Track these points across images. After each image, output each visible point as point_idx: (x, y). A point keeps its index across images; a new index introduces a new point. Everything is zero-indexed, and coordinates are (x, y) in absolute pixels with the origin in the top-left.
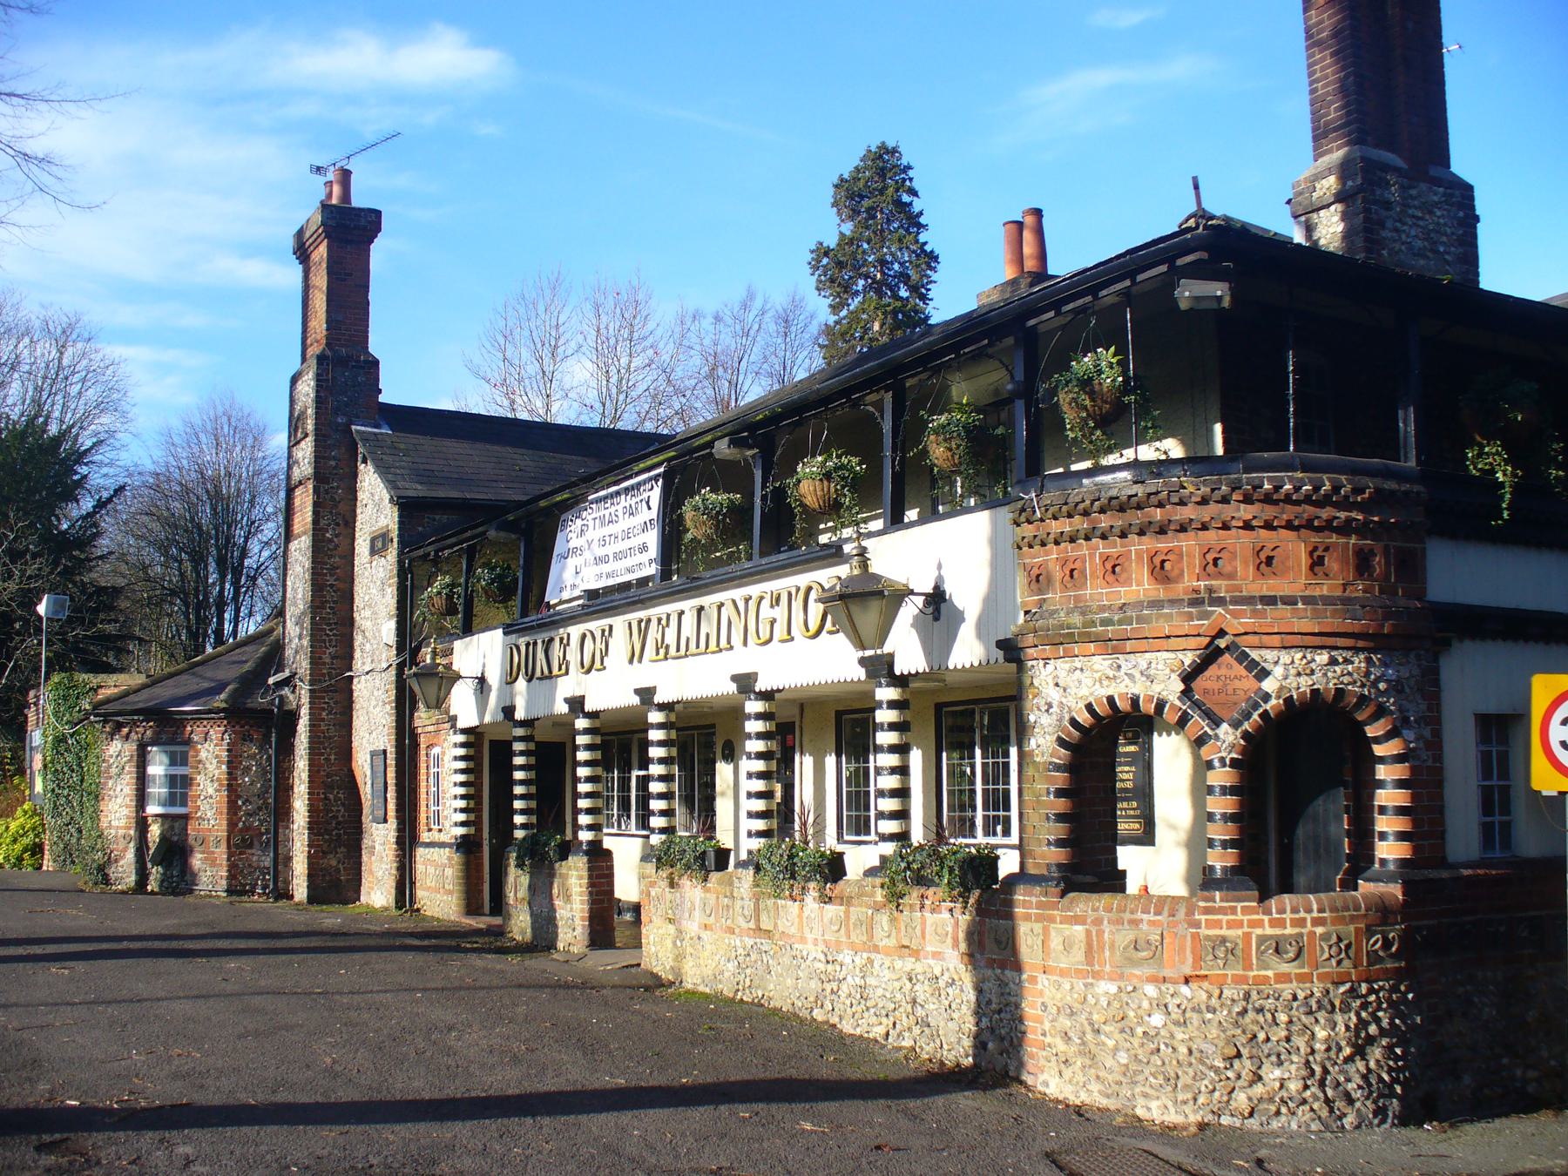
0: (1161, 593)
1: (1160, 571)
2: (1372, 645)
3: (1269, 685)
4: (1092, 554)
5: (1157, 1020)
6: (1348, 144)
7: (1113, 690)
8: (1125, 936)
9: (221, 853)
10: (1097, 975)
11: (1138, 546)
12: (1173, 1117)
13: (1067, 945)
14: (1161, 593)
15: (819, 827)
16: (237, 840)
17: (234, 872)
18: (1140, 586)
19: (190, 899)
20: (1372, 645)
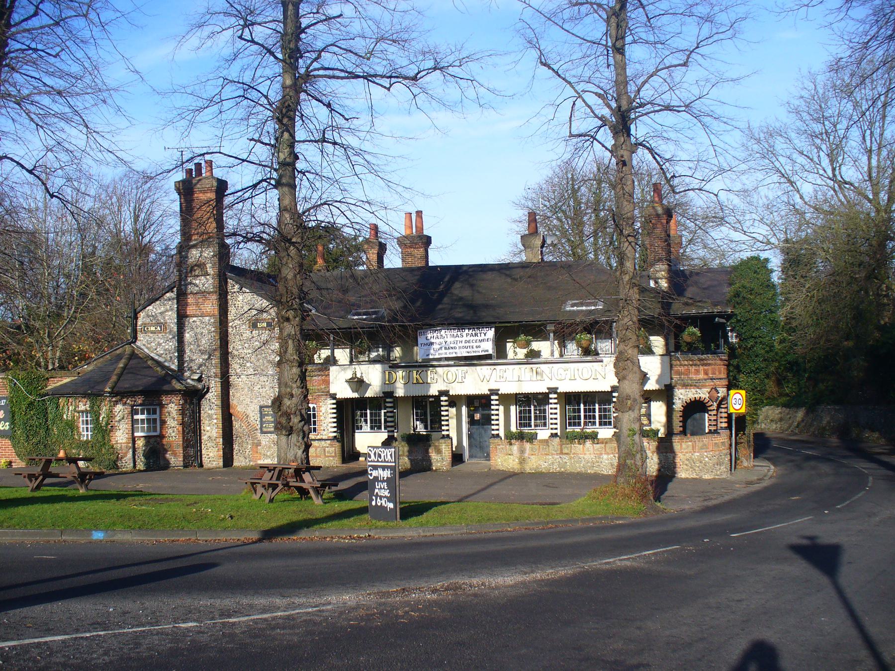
0: (706, 377)
1: (706, 373)
2: (875, 456)
3: (719, 395)
4: (693, 369)
5: (707, 459)
6: (792, 404)
7: (696, 396)
8: (701, 444)
9: (180, 451)
10: (695, 452)
11: (701, 368)
12: (710, 478)
13: (688, 447)
14: (706, 377)
15: (191, 452)
16: (185, 444)
17: (185, 457)
18: (701, 376)
19: (169, 471)
20: (875, 456)
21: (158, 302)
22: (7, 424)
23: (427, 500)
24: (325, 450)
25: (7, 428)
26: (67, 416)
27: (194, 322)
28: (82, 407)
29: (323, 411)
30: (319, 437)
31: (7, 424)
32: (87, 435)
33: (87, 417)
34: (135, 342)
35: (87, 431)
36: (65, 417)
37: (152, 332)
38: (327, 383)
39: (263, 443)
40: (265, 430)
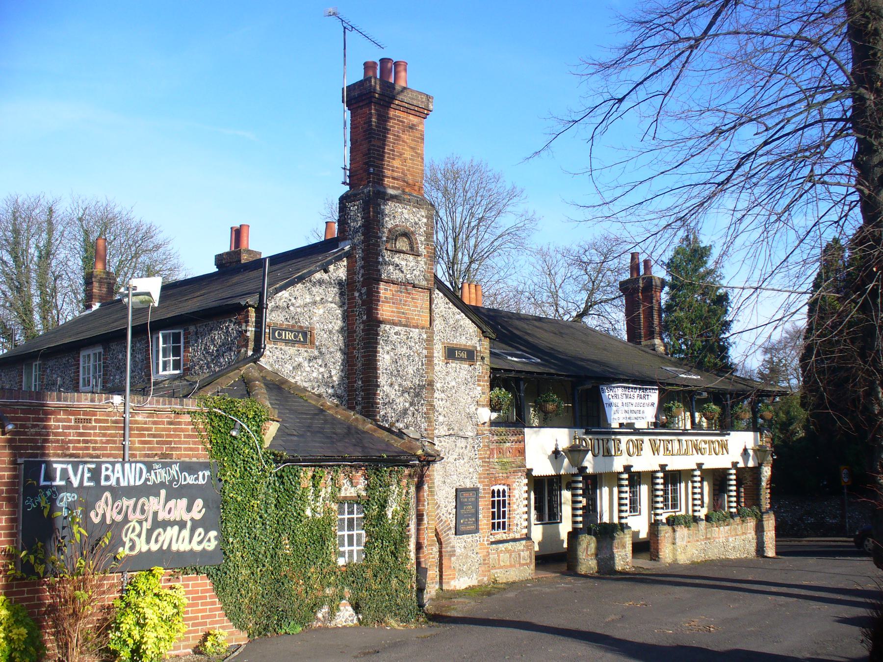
21: (299, 286)
22: (213, 534)
23: (844, 625)
24: (519, 555)
25: (212, 545)
26: (314, 510)
27: (396, 333)
28: (348, 491)
29: (517, 496)
30: (512, 536)
31: (213, 534)
32: (351, 553)
33: (351, 512)
34: (258, 359)
35: (351, 543)
36: (308, 512)
37: (287, 342)
38: (522, 452)
39: (458, 551)
40: (462, 528)
